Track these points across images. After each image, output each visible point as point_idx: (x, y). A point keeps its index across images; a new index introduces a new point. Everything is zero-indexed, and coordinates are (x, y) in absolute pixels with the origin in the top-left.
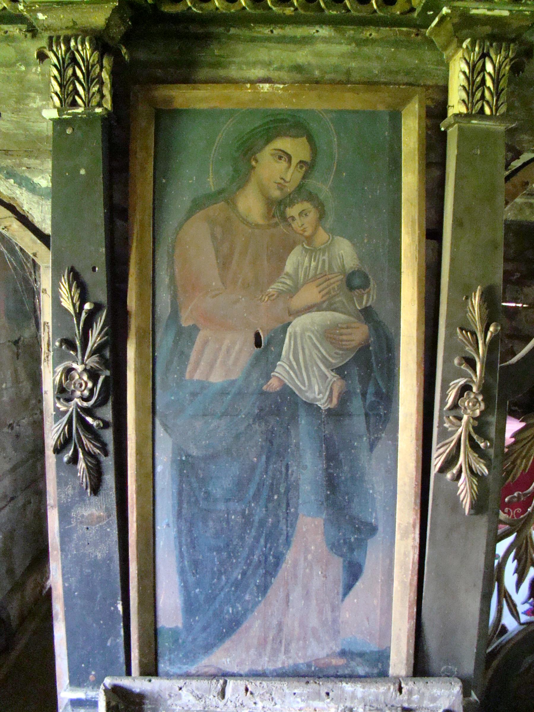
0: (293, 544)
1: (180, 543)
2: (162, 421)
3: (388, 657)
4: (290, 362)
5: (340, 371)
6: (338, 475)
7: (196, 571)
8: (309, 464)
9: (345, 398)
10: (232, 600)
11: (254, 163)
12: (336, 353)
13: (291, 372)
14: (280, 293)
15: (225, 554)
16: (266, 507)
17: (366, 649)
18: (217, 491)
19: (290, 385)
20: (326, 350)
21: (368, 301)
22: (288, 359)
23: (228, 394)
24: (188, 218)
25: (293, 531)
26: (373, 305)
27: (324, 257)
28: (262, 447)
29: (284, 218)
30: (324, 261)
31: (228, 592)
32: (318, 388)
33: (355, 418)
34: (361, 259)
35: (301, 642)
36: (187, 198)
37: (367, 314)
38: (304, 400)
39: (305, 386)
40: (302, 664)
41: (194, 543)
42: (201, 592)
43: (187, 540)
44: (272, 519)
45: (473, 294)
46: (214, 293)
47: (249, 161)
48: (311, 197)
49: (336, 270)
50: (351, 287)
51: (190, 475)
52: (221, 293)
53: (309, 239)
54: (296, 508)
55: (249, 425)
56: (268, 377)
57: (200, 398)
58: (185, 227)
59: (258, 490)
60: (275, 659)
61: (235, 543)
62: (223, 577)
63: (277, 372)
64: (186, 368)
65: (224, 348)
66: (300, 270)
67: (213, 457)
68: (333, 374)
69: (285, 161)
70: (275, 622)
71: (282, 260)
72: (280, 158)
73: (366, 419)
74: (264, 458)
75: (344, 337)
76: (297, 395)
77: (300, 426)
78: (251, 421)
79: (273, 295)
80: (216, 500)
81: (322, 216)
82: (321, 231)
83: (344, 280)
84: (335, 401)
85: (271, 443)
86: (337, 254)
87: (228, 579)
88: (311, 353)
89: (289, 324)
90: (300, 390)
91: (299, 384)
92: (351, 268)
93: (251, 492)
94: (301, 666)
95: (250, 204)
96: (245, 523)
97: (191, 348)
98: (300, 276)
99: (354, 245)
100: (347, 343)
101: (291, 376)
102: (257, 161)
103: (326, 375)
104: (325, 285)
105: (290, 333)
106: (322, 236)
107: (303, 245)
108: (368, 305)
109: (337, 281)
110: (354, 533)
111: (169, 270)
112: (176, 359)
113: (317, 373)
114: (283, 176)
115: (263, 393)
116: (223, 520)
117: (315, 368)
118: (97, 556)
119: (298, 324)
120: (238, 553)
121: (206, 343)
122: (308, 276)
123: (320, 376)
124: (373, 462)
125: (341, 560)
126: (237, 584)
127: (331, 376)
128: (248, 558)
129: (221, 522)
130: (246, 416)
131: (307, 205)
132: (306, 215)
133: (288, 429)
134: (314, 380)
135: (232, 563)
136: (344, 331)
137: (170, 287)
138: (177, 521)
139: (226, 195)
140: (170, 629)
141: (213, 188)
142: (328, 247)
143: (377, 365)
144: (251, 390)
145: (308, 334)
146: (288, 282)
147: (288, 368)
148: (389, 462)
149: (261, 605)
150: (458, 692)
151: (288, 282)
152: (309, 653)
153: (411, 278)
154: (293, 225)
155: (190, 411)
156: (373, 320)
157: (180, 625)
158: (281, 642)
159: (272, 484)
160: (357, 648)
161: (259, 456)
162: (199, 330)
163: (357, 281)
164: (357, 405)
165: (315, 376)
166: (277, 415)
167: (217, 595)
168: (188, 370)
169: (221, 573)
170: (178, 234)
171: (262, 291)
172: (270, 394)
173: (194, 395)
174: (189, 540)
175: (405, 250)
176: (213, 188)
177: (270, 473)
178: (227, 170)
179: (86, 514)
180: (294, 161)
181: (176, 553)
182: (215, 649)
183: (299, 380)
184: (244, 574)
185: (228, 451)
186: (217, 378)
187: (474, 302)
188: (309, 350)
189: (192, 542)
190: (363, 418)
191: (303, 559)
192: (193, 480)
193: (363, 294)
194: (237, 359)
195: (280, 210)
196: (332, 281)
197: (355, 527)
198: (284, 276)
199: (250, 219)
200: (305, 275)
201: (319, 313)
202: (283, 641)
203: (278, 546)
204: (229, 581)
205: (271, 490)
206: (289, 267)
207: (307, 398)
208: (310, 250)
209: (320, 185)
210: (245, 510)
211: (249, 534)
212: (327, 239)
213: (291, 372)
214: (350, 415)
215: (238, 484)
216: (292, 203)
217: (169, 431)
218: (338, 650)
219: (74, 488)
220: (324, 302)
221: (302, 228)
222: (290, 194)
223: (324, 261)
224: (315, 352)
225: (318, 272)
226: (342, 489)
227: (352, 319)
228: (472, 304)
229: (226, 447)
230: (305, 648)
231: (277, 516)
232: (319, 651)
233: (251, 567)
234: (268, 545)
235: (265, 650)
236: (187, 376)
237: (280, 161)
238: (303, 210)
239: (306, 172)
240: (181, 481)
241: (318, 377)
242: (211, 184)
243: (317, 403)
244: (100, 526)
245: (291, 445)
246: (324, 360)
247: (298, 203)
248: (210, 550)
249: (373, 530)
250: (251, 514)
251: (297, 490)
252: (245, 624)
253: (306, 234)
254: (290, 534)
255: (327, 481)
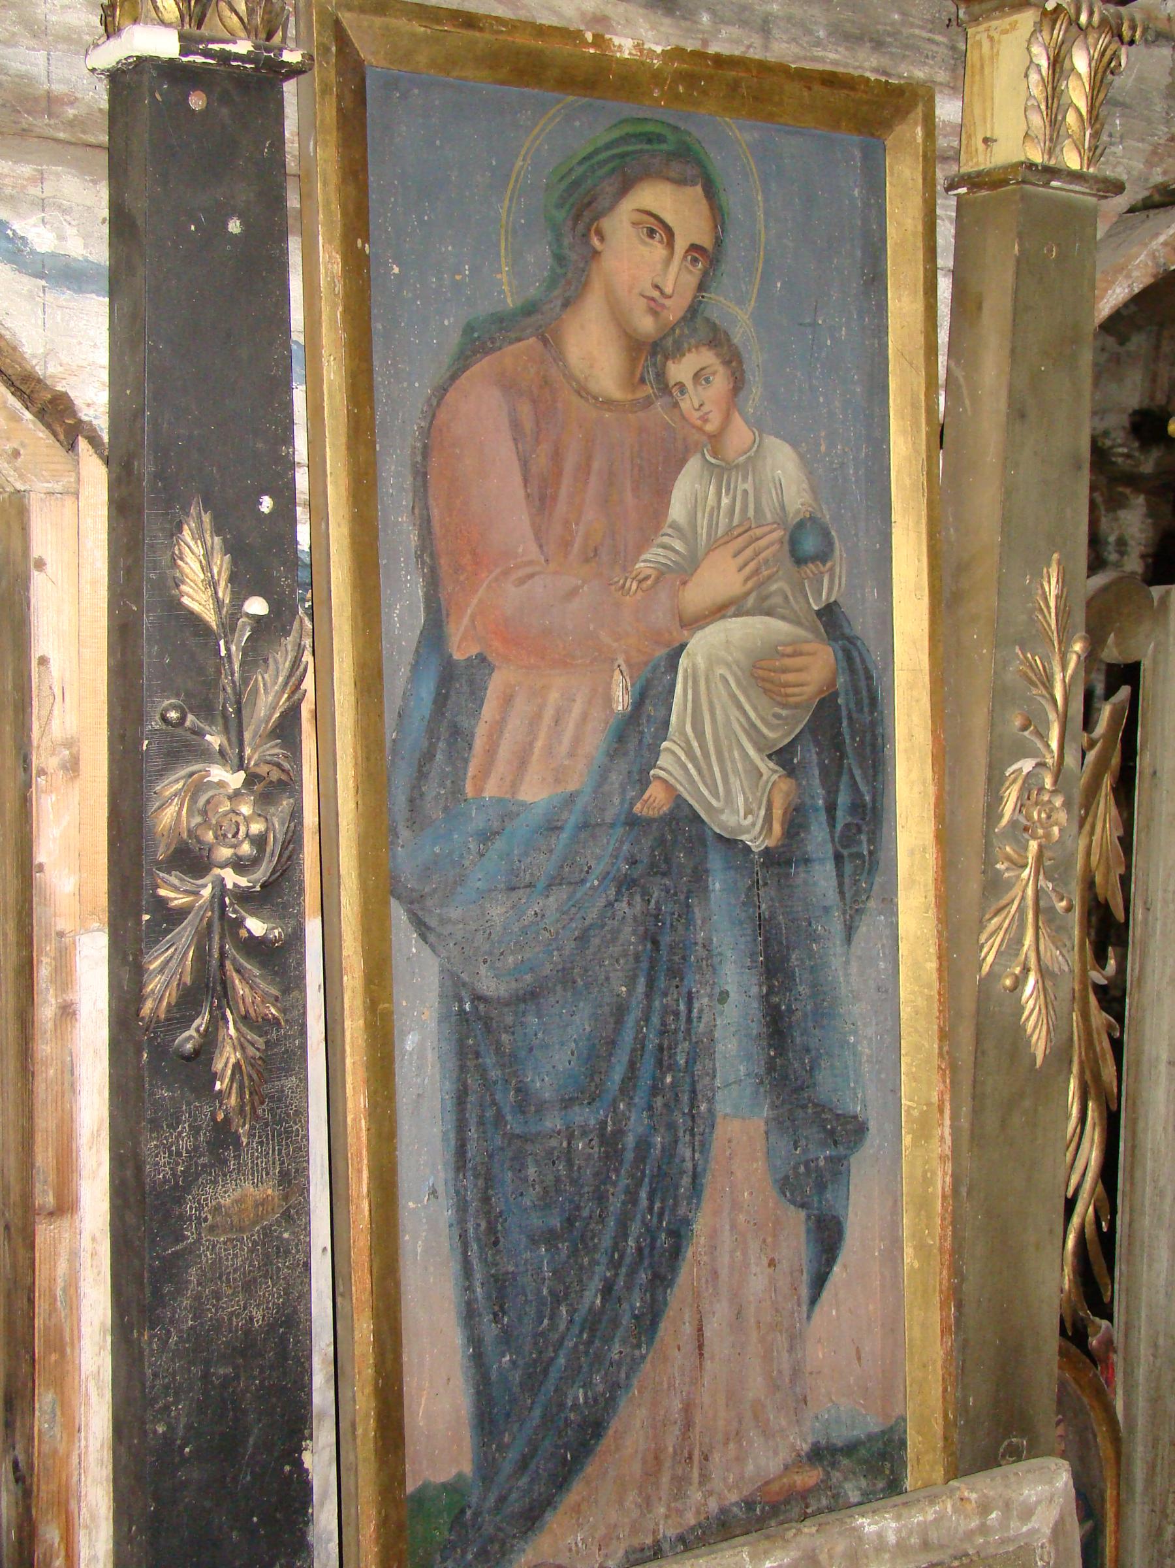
0: (706, 1194)
1: (463, 1236)
2: (415, 914)
3: (903, 1444)
4: (688, 742)
5: (783, 757)
6: (789, 1007)
7: (502, 1308)
8: (731, 988)
9: (795, 824)
10: (585, 1369)
11: (595, 242)
12: (777, 716)
13: (690, 766)
14: (662, 573)
15: (564, 1247)
16: (650, 1108)
17: (859, 1433)
18: (544, 1082)
19: (688, 798)
20: (755, 709)
21: (830, 589)
22: (683, 733)
23: (560, 828)
24: (454, 378)
25: (706, 1161)
26: (841, 601)
27: (746, 486)
28: (637, 959)
29: (664, 387)
30: (745, 492)
31: (576, 1345)
32: (742, 803)
33: (817, 867)
34: (814, 490)
35: (731, 1445)
36: (452, 320)
37: (830, 619)
38: (718, 831)
39: (718, 798)
40: (737, 1504)
41: (496, 1233)
42: (513, 1362)
43: (479, 1225)
44: (663, 1138)
45: (1045, 570)
46: (521, 573)
47: (585, 236)
48: (717, 339)
49: (769, 516)
50: (799, 560)
51: (482, 1048)
52: (539, 573)
53: (716, 440)
54: (711, 1101)
55: (610, 904)
56: (644, 782)
57: (499, 844)
58: (450, 397)
59: (632, 1065)
60: (679, 1505)
61: (585, 1213)
62: (563, 1309)
63: (661, 768)
64: (465, 769)
65: (549, 714)
66: (699, 515)
67: (532, 996)
68: (771, 765)
69: (661, 242)
70: (677, 1405)
71: (663, 494)
72: (651, 233)
73: (837, 866)
74: (641, 988)
75: (790, 677)
76: (703, 821)
77: (712, 895)
78: (612, 892)
79: (647, 578)
80: (541, 1108)
81: (738, 384)
82: (737, 420)
83: (787, 538)
84: (777, 828)
85: (656, 943)
86: (769, 475)
87: (572, 1311)
88: (727, 716)
89: (683, 646)
90: (709, 807)
91: (706, 793)
92: (798, 512)
93: (617, 1075)
94: (735, 1509)
95: (592, 349)
96: (607, 1156)
97: (476, 713)
98: (699, 529)
99: (801, 457)
100: (796, 690)
101: (690, 775)
102: (602, 239)
103: (757, 769)
104: (749, 552)
105: (686, 671)
106: (740, 435)
107: (703, 455)
108: (832, 600)
109: (772, 544)
110: (823, 1145)
111: (417, 511)
112: (442, 745)
113: (740, 766)
114: (658, 281)
115: (633, 821)
116: (558, 1158)
117: (736, 754)
118: (251, 1318)
119: (703, 646)
120: (592, 1239)
121: (507, 700)
122: (716, 533)
123: (745, 771)
124: (854, 968)
125: (802, 1214)
126: (593, 1322)
127: (766, 767)
128: (615, 1247)
129: (554, 1163)
130: (601, 882)
131: (705, 358)
132: (707, 380)
133: (688, 906)
134: (735, 783)
135: (581, 1267)
136: (788, 662)
137: (421, 556)
138: (456, 1179)
139: (536, 321)
140: (444, 1486)
141: (509, 301)
142: (752, 463)
143: (853, 738)
144: (609, 817)
145: (721, 670)
146: (678, 545)
147: (683, 758)
148: (882, 965)
149: (646, 1366)
150: (1066, 1484)
151: (678, 545)
152: (750, 1468)
153: (912, 534)
154: (683, 405)
155: (477, 880)
156: (843, 634)
157: (467, 1468)
158: (690, 1457)
159: (661, 1048)
160: (841, 1435)
161: (631, 982)
162: (492, 669)
163: (810, 544)
164: (818, 838)
165: (736, 772)
166: (664, 874)
167: (552, 1359)
168: (471, 771)
169: (557, 1300)
170: (434, 416)
171: (624, 569)
172: (650, 821)
173: (487, 837)
174: (484, 1225)
175: (898, 472)
176: (509, 301)
177: (655, 1020)
178: (539, 256)
179: (226, 1201)
180: (681, 245)
181: (455, 1267)
182: (549, 1516)
183: (705, 783)
184: (607, 1290)
185: (565, 977)
186: (535, 792)
187: (1047, 589)
188: (724, 708)
189: (491, 1229)
190: (830, 866)
191: (727, 1227)
192: (489, 1060)
193: (822, 573)
194: (577, 740)
195: (654, 365)
196: (762, 543)
197: (824, 1127)
198: (669, 531)
199: (593, 387)
200: (710, 527)
201: (739, 619)
202: (696, 1453)
203: (675, 1205)
204: (576, 1317)
205: (659, 1063)
206: (677, 510)
207: (722, 825)
208: (718, 466)
209: (735, 310)
210: (606, 1123)
211: (614, 1184)
212: (749, 441)
213: (690, 766)
214: (807, 861)
215: (589, 1058)
216: (678, 351)
217: (432, 938)
218: (806, 1447)
219: (195, 1130)
220: (748, 594)
221: (700, 413)
222: (673, 329)
223: (745, 492)
224: (734, 713)
225: (736, 522)
226: (798, 1040)
227: (802, 633)
228: (1044, 593)
229: (560, 967)
230: (740, 1459)
231: (671, 1127)
232: (766, 1460)
233: (624, 1270)
234: (657, 1205)
235: (657, 1489)
236: (469, 790)
237: (651, 241)
238: (702, 369)
239: (705, 274)
240: (463, 1068)
241: (743, 776)
242: (506, 288)
243: (743, 838)
244: (264, 1228)
245: (696, 944)
246: (753, 731)
247: (690, 350)
248: (534, 1242)
249: (856, 1130)
250: (619, 1133)
251: (712, 1055)
252: (614, 1425)
253: (709, 428)
254: (699, 1170)
255: (767, 1025)
